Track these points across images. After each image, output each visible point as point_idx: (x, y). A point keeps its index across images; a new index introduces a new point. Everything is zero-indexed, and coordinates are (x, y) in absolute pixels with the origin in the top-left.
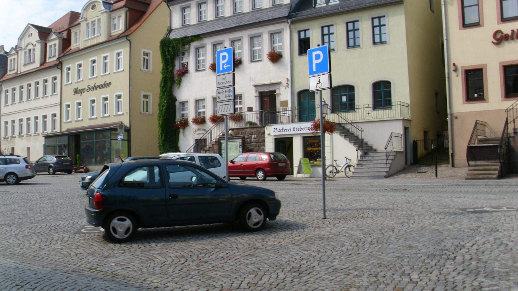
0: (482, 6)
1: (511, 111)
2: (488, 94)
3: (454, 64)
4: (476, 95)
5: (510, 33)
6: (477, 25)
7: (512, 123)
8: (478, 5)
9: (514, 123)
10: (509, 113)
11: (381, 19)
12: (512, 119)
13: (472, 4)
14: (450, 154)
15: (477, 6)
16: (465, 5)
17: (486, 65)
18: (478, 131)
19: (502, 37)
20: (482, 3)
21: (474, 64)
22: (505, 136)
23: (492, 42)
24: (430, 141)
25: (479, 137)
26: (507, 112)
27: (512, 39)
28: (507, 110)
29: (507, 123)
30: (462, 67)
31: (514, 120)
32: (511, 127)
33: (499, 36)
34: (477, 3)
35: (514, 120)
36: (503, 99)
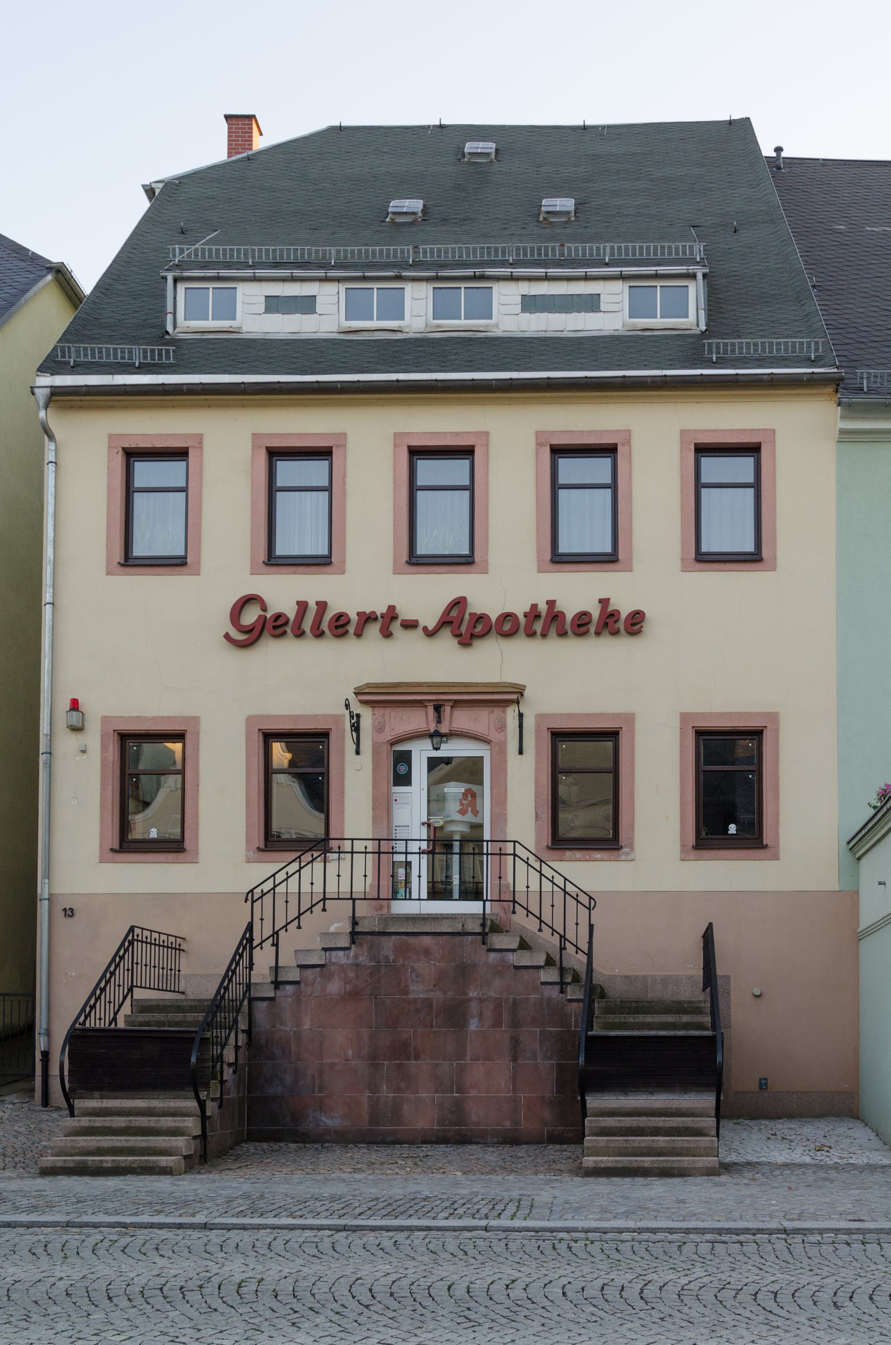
0: (200, 494)
1: (268, 899)
2: (197, 829)
3: (75, 705)
4: (732, 829)
5: (291, 613)
6: (178, 563)
7: (268, 944)
8: (329, 489)
9: (276, 945)
10: (257, 905)
11: (326, 494)
12: (268, 932)
13: (587, 481)
14: (38, 1056)
15: (467, 494)
16: (280, 483)
17: (685, 717)
18: (137, 969)
19: (262, 620)
20: (201, 485)
21: (151, 713)
22: (235, 991)
23: (227, 636)
24: (273, 995)
25: (139, 994)
26: (253, 902)
27: (300, 634)
28: (250, 897)
29: (247, 942)
30: (105, 720)
31: (276, 934)
32: (263, 958)
33: (250, 616)
34: (326, 483)
35: (276, 934)
36: (251, 854)
